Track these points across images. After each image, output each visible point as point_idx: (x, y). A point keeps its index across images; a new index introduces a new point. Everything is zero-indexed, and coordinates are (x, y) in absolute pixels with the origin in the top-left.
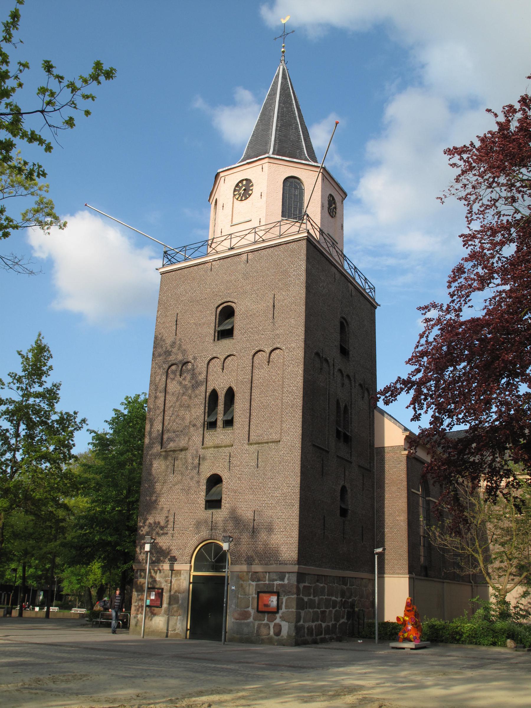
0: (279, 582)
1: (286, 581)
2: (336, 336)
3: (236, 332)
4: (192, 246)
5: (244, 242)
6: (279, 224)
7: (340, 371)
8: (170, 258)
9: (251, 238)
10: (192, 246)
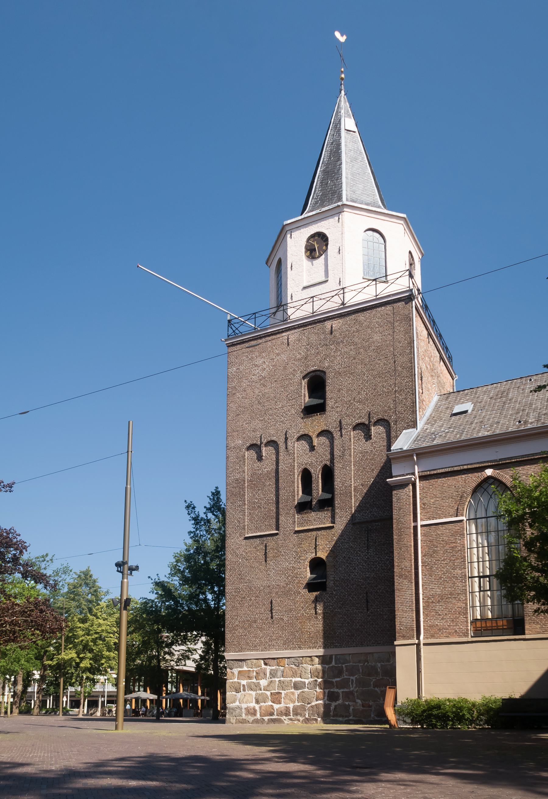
8: (234, 329)
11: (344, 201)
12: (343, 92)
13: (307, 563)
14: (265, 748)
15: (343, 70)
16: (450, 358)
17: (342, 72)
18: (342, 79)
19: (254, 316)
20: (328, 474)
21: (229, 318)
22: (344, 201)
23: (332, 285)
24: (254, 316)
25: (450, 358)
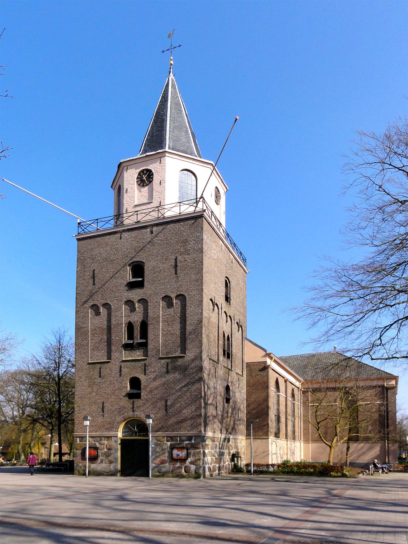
0: (187, 442)
1: (193, 441)
2: (223, 289)
3: (146, 283)
4: (103, 220)
5: (148, 218)
6: (136, 213)
7: (225, 312)
8: (83, 228)
9: (155, 215)
10: (103, 220)
11: (167, 149)
12: (171, 74)
13: (129, 378)
14: (361, 462)
15: (172, 58)
16: (244, 260)
17: (171, 59)
18: (171, 65)
19: (157, 209)
20: (144, 326)
21: (79, 221)
22: (167, 149)
23: (155, 204)
24: (136, 213)
25: (244, 260)
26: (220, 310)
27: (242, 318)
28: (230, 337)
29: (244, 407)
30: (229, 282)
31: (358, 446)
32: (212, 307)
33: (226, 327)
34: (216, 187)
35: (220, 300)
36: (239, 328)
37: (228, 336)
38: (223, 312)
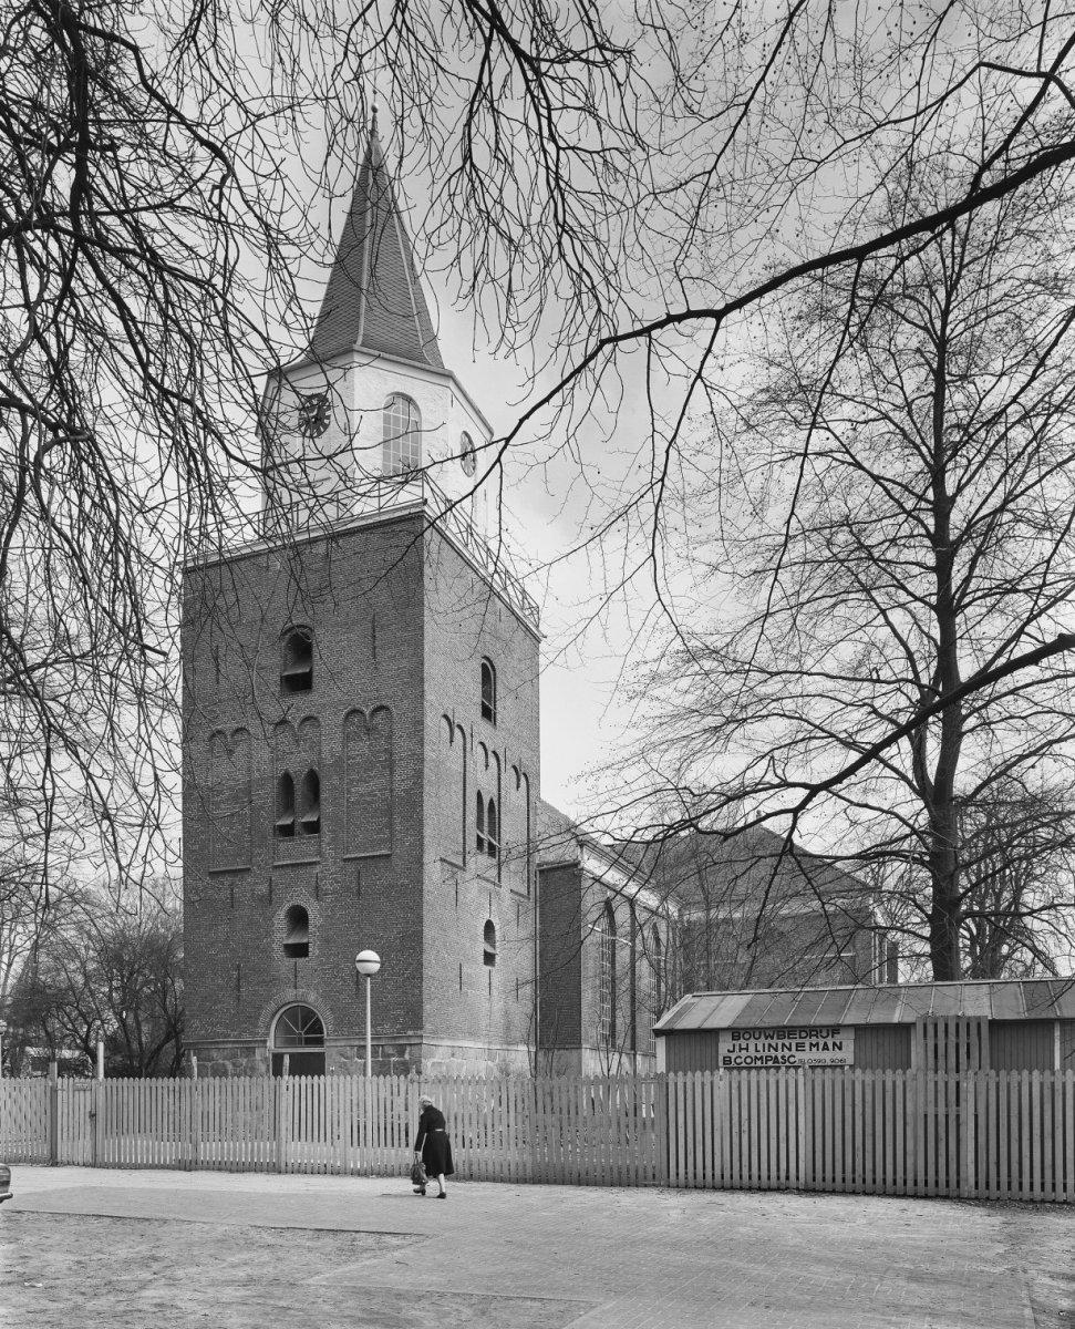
26: (468, 740)
27: (526, 755)
28: (496, 804)
29: (957, 1220)
30: (493, 666)
31: (233, 325)
32: (446, 735)
33: (484, 780)
34: (466, 434)
35: (470, 715)
36: (518, 780)
37: (491, 802)
38: (476, 743)
